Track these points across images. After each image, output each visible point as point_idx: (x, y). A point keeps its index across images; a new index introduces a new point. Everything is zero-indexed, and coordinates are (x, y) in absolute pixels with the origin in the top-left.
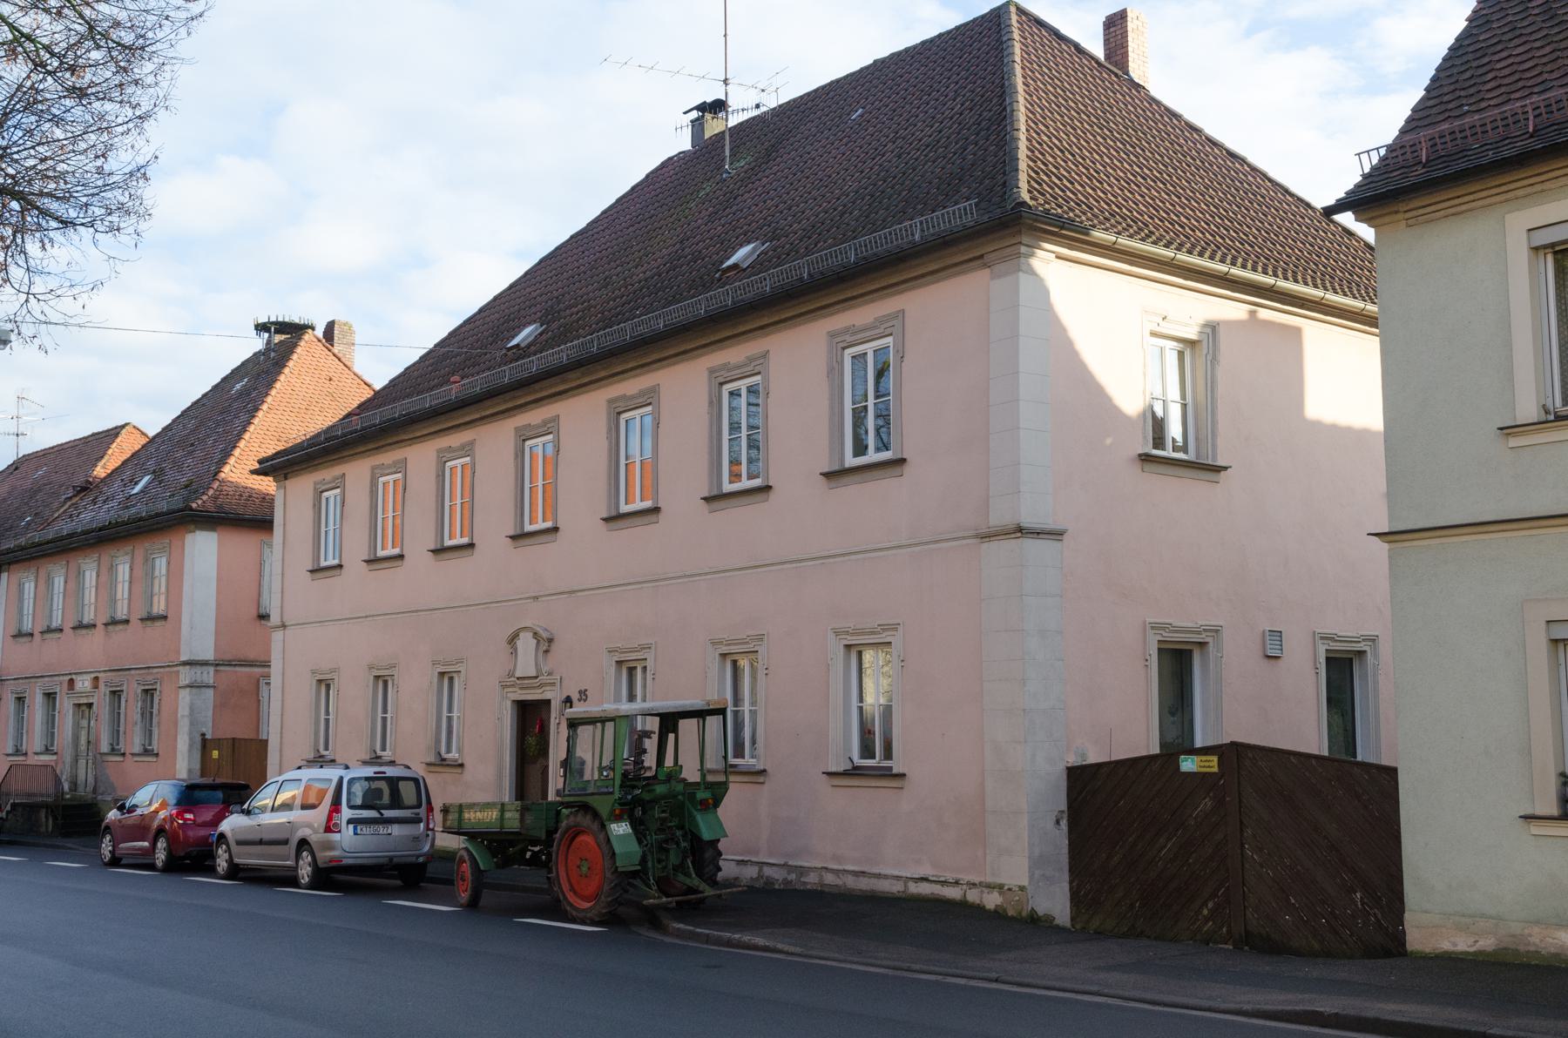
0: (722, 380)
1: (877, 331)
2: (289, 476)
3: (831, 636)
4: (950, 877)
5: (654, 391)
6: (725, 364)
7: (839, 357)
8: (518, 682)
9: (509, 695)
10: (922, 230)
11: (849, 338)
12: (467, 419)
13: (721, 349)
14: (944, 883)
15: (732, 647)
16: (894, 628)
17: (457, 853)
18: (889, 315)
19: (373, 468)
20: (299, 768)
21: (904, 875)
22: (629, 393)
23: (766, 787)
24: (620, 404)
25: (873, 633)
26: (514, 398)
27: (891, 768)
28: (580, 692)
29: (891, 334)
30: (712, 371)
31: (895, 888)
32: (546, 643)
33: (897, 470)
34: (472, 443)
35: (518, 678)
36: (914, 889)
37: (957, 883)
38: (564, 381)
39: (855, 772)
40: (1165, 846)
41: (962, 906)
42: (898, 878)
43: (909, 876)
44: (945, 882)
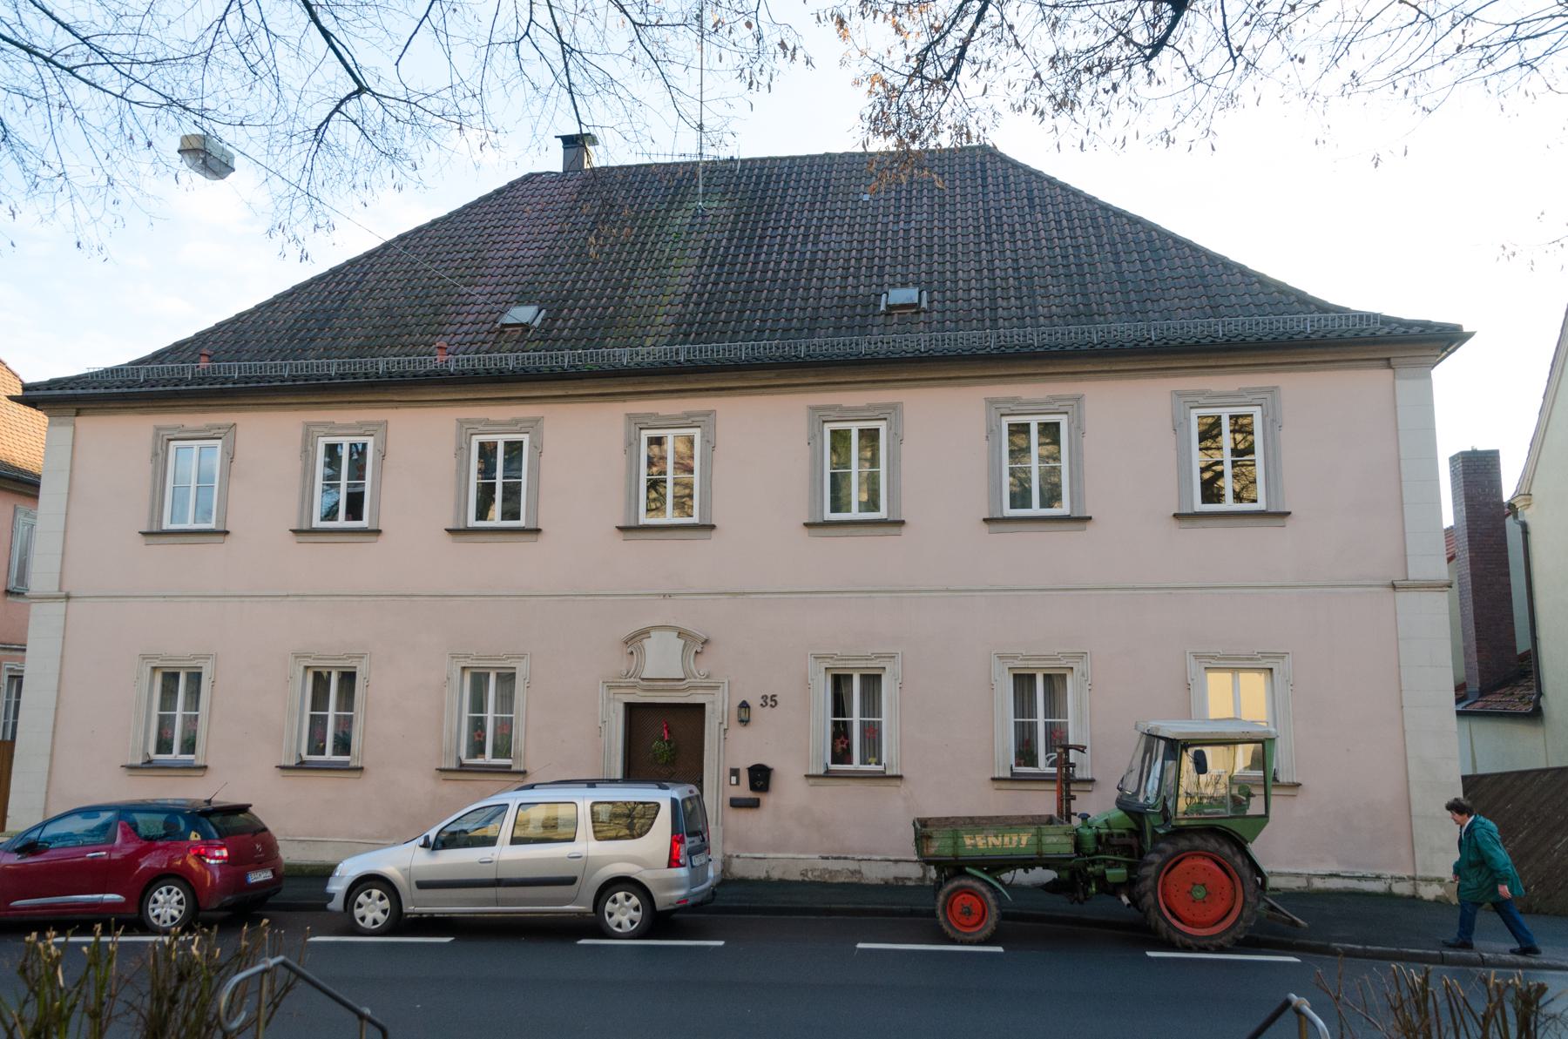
0: (824, 419)
1: (1243, 400)
2: (82, 412)
3: (811, 660)
4: (1368, 872)
5: (1078, 399)
6: (1015, 398)
7: (164, 448)
8: (641, 682)
9: (616, 696)
10: (239, 373)
11: (1202, 400)
12: (538, 393)
13: (729, 396)
14: (1360, 878)
15: (1030, 662)
16: (1282, 656)
17: (599, 868)
18: (1261, 388)
19: (308, 426)
20: (1122, 781)
21: (1306, 871)
22: (845, 404)
23: (1093, 795)
24: (832, 413)
25: (1252, 659)
26: (644, 383)
27: (510, 766)
28: (765, 697)
29: (885, 419)
30: (158, 429)
31: (1299, 884)
32: (695, 644)
33: (895, 530)
34: (537, 420)
35: (643, 679)
36: (1318, 884)
37: (1378, 878)
38: (779, 377)
39: (463, 768)
40: (1561, 841)
41: (1389, 896)
42: (1297, 875)
43: (1312, 872)
44: (1363, 877)
